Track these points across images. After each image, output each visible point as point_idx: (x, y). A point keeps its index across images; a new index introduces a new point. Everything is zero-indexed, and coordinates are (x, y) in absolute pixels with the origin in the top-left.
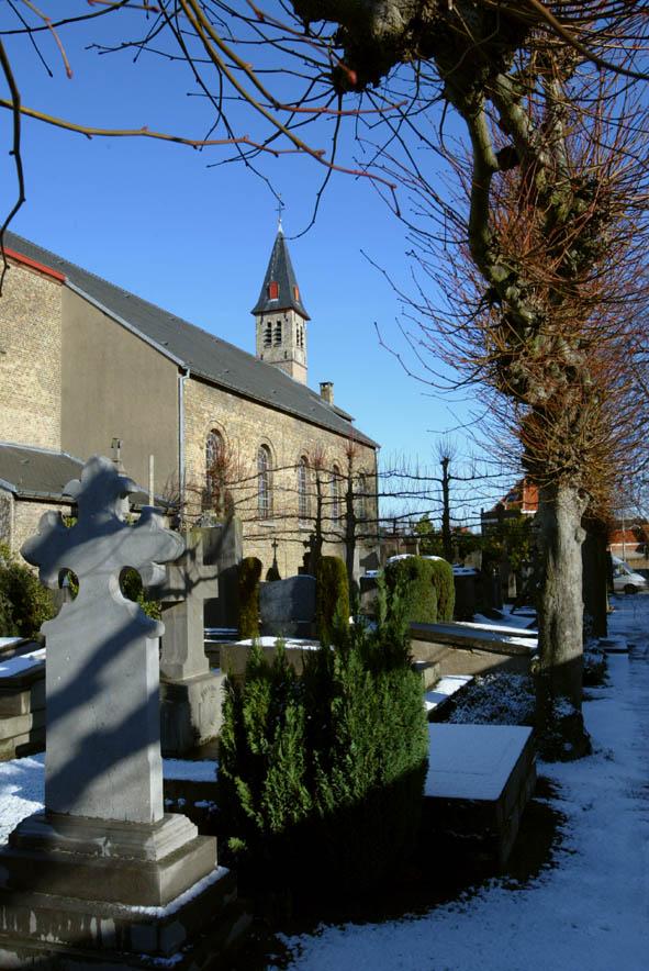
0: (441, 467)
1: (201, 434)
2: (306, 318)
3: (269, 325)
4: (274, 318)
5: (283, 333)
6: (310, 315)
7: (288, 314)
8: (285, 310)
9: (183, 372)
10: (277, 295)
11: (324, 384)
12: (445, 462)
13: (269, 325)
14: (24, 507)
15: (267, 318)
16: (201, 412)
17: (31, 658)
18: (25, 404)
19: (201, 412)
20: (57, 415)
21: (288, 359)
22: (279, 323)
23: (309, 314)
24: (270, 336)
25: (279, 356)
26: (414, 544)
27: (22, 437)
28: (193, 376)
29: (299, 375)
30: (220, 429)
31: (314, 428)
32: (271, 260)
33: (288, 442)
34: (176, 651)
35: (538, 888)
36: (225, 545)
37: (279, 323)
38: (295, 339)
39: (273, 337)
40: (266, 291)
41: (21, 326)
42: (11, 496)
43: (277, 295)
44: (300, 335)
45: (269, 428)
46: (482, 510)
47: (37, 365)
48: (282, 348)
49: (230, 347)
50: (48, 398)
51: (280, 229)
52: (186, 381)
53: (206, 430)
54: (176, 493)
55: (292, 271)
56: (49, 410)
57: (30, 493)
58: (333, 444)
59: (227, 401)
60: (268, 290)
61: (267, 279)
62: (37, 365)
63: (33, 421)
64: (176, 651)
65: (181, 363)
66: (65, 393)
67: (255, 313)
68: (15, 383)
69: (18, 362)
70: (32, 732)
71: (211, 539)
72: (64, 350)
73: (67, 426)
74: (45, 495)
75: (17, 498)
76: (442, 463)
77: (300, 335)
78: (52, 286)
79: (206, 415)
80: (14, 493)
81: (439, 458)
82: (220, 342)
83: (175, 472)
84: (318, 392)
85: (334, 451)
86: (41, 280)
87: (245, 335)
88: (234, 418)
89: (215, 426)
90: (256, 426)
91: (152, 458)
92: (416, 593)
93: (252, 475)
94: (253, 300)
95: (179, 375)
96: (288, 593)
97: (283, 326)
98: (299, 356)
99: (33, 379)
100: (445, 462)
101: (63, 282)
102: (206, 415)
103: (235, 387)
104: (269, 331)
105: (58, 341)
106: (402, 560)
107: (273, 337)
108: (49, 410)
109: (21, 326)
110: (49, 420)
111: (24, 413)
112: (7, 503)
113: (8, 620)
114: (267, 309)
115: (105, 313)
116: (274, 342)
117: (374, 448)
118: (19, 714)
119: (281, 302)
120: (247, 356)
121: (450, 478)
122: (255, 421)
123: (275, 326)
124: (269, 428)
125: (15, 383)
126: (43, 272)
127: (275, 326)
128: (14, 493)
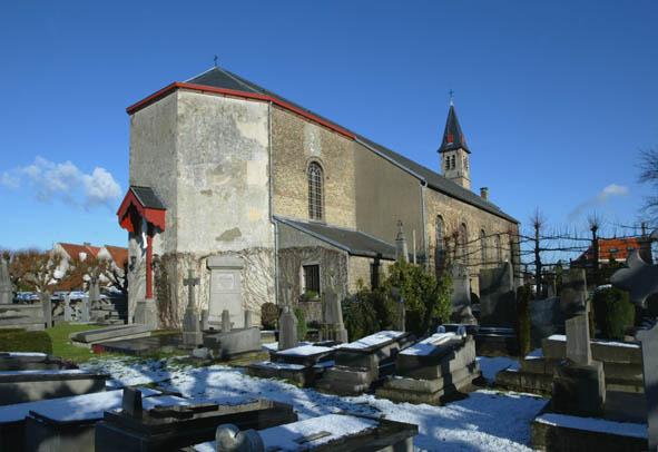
1: (433, 218)
2: (468, 152)
9: (423, 183)
10: (453, 141)
12: (594, 229)
14: (353, 259)
16: (432, 205)
20: (354, 210)
21: (460, 176)
23: (470, 149)
28: (429, 186)
29: (466, 185)
35: (318, 416)
36: (504, 279)
39: (451, 164)
40: (446, 139)
43: (453, 141)
45: (466, 213)
47: (344, 184)
48: (456, 171)
50: (349, 201)
52: (425, 189)
57: (356, 252)
61: (446, 132)
65: (423, 178)
66: (357, 199)
67: (440, 151)
70: (444, 387)
73: (359, 216)
74: (362, 252)
78: (349, 142)
81: (589, 226)
85: (499, 226)
87: (436, 164)
96: (549, 307)
98: (466, 175)
100: (594, 229)
101: (354, 139)
103: (449, 191)
107: (451, 164)
112: (345, 257)
120: (438, 175)
124: (466, 213)
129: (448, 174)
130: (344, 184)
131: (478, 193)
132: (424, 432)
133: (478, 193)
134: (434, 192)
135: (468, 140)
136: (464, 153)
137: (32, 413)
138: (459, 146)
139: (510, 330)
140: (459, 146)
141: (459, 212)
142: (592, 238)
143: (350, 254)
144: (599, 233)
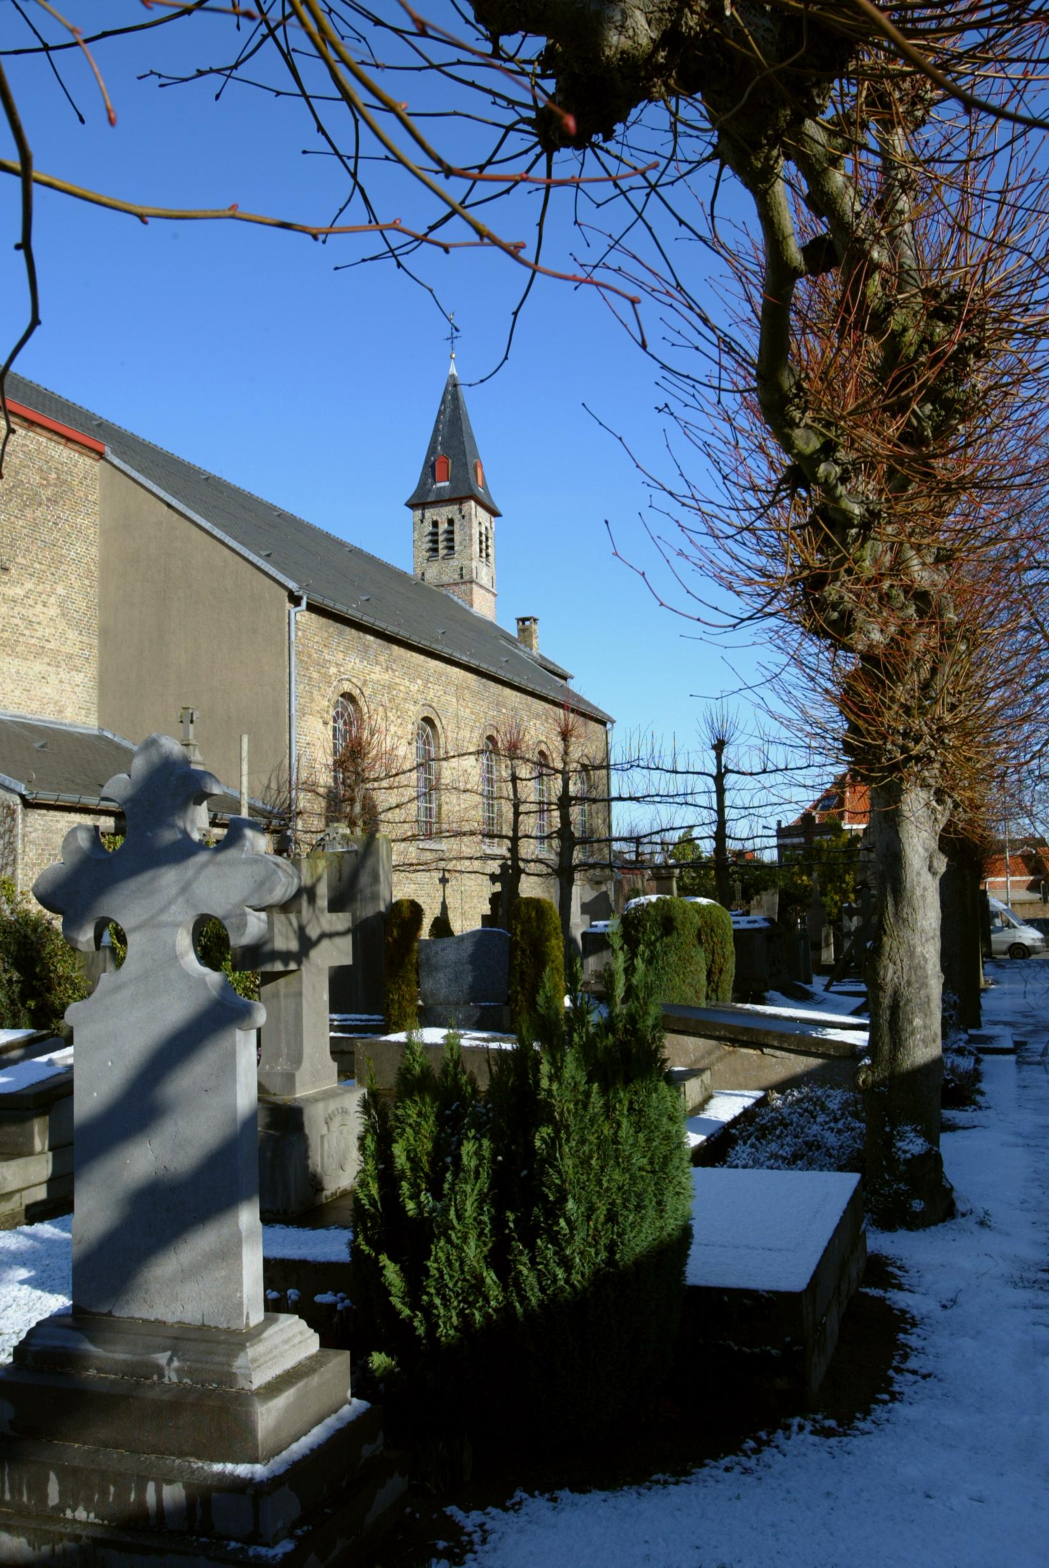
0: (713, 753)
1: (325, 701)
2: (494, 513)
3: (435, 524)
5: (457, 538)
8: (460, 500)
9: (295, 600)
10: (449, 477)
11: (523, 620)
12: (719, 746)
13: (435, 524)
14: (37, 818)
15: (430, 514)
16: (323, 665)
18: (39, 652)
20: (92, 670)
21: (466, 580)
22: (451, 522)
23: (500, 507)
24: (435, 542)
27: (35, 706)
28: (311, 608)
29: (483, 606)
31: (508, 691)
32: (438, 421)
33: (465, 713)
36: (364, 879)
37: (451, 522)
38: (476, 547)
39: (442, 543)
40: (430, 470)
41: (35, 525)
42: (18, 800)
43: (449, 477)
44: (484, 540)
48: (455, 563)
50: (76, 642)
51: (453, 370)
52: (301, 616)
55: (472, 437)
56: (78, 662)
57: (48, 797)
58: (537, 717)
60: (433, 467)
61: (432, 450)
63: (53, 679)
65: (292, 585)
66: (105, 634)
67: (412, 505)
68: (23, 618)
69: (29, 585)
72: (105, 565)
73: (109, 687)
75: (28, 804)
76: (714, 747)
77: (484, 540)
78: (84, 463)
79: (333, 670)
80: (22, 797)
81: (709, 740)
85: (539, 727)
87: (394, 539)
88: (378, 674)
89: (347, 687)
92: (673, 958)
95: (289, 606)
97: (456, 528)
98: (484, 575)
99: (53, 611)
100: (719, 746)
101: (101, 455)
102: (333, 670)
103: (380, 625)
104: (435, 534)
105: (94, 550)
107: (442, 543)
109: (35, 525)
110: (79, 678)
111: (39, 667)
112: (11, 813)
114: (431, 498)
115: (169, 506)
116: (442, 552)
117: (604, 724)
119: (453, 488)
120: (401, 576)
121: (728, 771)
123: (443, 527)
125: (23, 618)
126: (69, 439)
128: (22, 797)
129: (434, 572)
130: (60, 590)
131: (513, 630)
132: (509, 1214)
133: (513, 630)
134: (334, 627)
135: (494, 465)
136: (483, 515)
137: (664, 1006)
138: (464, 493)
139: (381, 1017)
140: (464, 493)
141: (414, 688)
142: (714, 772)
143: (28, 804)
144: (729, 752)
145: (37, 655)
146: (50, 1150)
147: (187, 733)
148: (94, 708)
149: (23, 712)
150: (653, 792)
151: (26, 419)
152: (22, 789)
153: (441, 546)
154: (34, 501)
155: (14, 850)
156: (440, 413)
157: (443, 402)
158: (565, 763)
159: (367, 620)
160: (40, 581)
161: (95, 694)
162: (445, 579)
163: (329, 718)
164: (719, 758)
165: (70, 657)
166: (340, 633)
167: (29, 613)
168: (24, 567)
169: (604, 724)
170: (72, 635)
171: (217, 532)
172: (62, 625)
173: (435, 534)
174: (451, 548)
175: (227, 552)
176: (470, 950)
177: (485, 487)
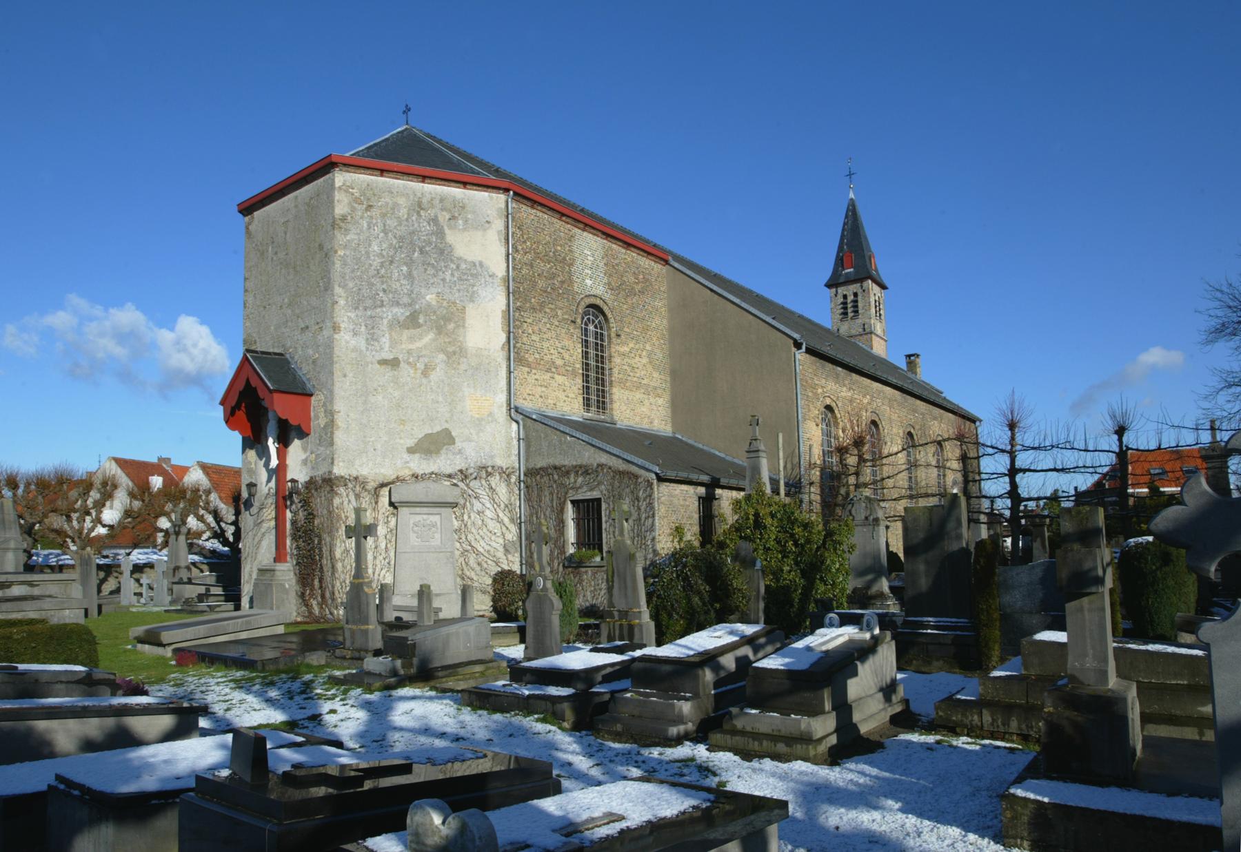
0: (1116, 437)
1: (816, 410)
2: (883, 287)
3: (845, 297)
4: (849, 290)
5: (860, 305)
6: (887, 284)
7: (865, 284)
8: (861, 280)
9: (798, 345)
10: (853, 265)
11: (909, 356)
12: (1120, 431)
13: (845, 297)
15: (841, 290)
16: (814, 387)
17: (809, 649)
18: (638, 386)
19: (814, 387)
21: (867, 332)
22: (856, 295)
23: (886, 282)
24: (845, 308)
25: (856, 329)
26: (1043, 525)
27: (637, 419)
28: (810, 351)
29: (878, 348)
30: (833, 405)
31: (918, 402)
32: (843, 230)
33: (894, 417)
34: (1091, 652)
35: (599, 784)
36: (951, 525)
37: (856, 295)
38: (873, 310)
39: (849, 309)
40: (840, 262)
41: (633, 308)
42: (654, 476)
43: (853, 265)
44: (878, 304)
46: (1076, 488)
48: (859, 321)
49: (809, 321)
50: (658, 379)
51: (852, 195)
52: (801, 356)
53: (820, 405)
54: (795, 473)
55: (866, 238)
56: (659, 391)
57: (671, 474)
58: (935, 419)
59: (837, 376)
60: (842, 259)
62: (648, 347)
63: (646, 402)
64: (1091, 652)
65: (796, 336)
67: (829, 285)
68: (629, 365)
69: (631, 345)
71: (931, 525)
72: (672, 331)
73: (677, 406)
75: (661, 479)
76: (1116, 432)
77: (878, 304)
79: (820, 391)
80: (657, 474)
81: (1111, 426)
82: (801, 317)
83: (793, 452)
84: (905, 368)
85: (941, 426)
86: (648, 262)
87: (821, 308)
88: (845, 393)
89: (828, 401)
90: (865, 401)
91: (781, 436)
92: (1171, 583)
93: (895, 449)
94: (827, 274)
95: (794, 349)
97: (860, 298)
98: (879, 329)
99: (645, 360)
102: (820, 391)
103: (847, 360)
104: (845, 303)
105: (665, 322)
106: (1148, 542)
107: (849, 309)
108: (659, 391)
109: (633, 308)
110: (660, 401)
111: (638, 395)
112: (650, 485)
113: (704, 604)
114: (842, 280)
115: (711, 290)
116: (851, 315)
117: (974, 422)
118: (823, 712)
119: (856, 272)
120: (828, 331)
121: (1128, 449)
122: (864, 396)
123: (851, 298)
125: (629, 365)
126: (649, 254)
127: (851, 298)
128: (657, 474)
129: (845, 329)
131: (902, 364)
133: (902, 364)
134: (819, 362)
136: (876, 289)
142: (1117, 450)
144: (1129, 439)
145: (638, 388)
146: (833, 709)
147: (754, 431)
148: (669, 420)
149: (632, 423)
150: (1081, 464)
151: (625, 243)
152: (657, 469)
153: (849, 311)
154: (632, 293)
155: (652, 508)
156: (845, 224)
157: (846, 217)
158: (1012, 446)
159: (839, 356)
160: (637, 343)
161: (669, 411)
162: (853, 332)
163: (819, 421)
164: (1120, 440)
165: (655, 388)
166: (823, 367)
167: (632, 362)
168: (629, 334)
169: (974, 422)
170: (656, 375)
171: (744, 305)
172: (650, 368)
173: (845, 303)
174: (856, 312)
175: (751, 317)
176: (1040, 575)
177: (876, 270)
